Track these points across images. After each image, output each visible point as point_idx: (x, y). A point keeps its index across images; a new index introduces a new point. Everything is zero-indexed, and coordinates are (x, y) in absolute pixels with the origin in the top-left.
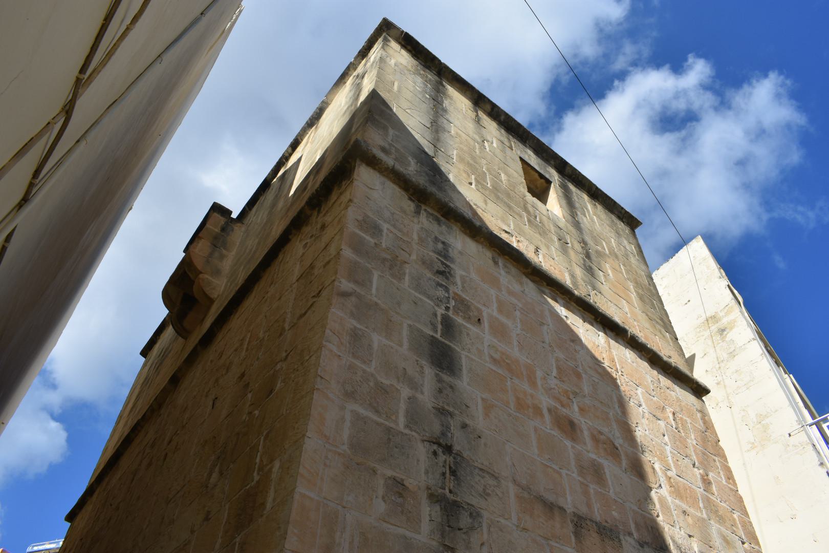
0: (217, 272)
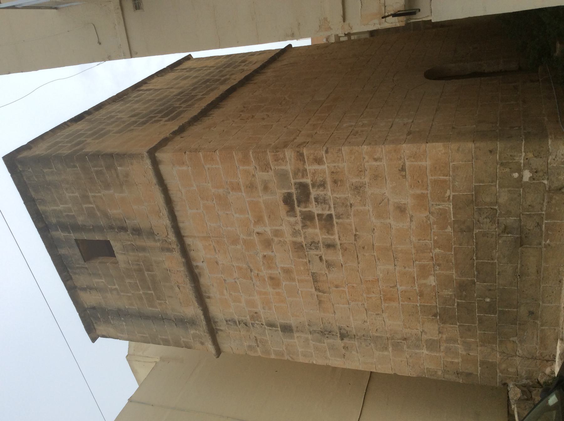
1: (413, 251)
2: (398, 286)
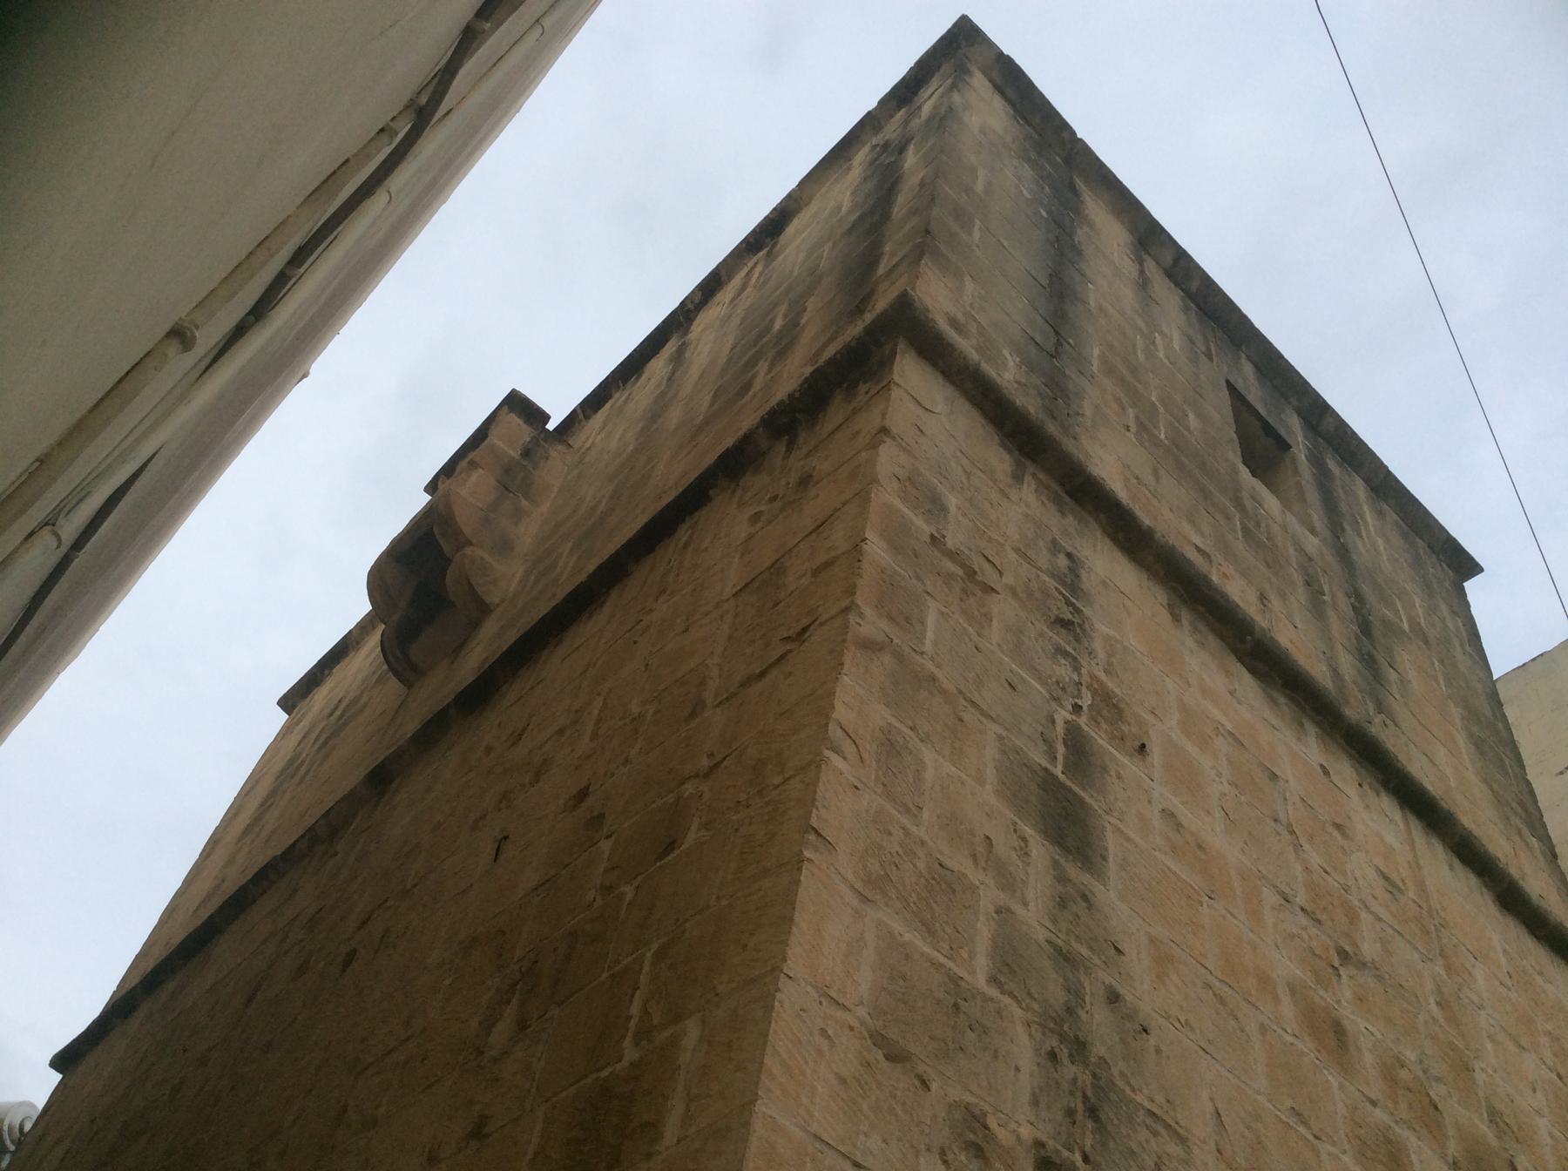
0: (504, 547)
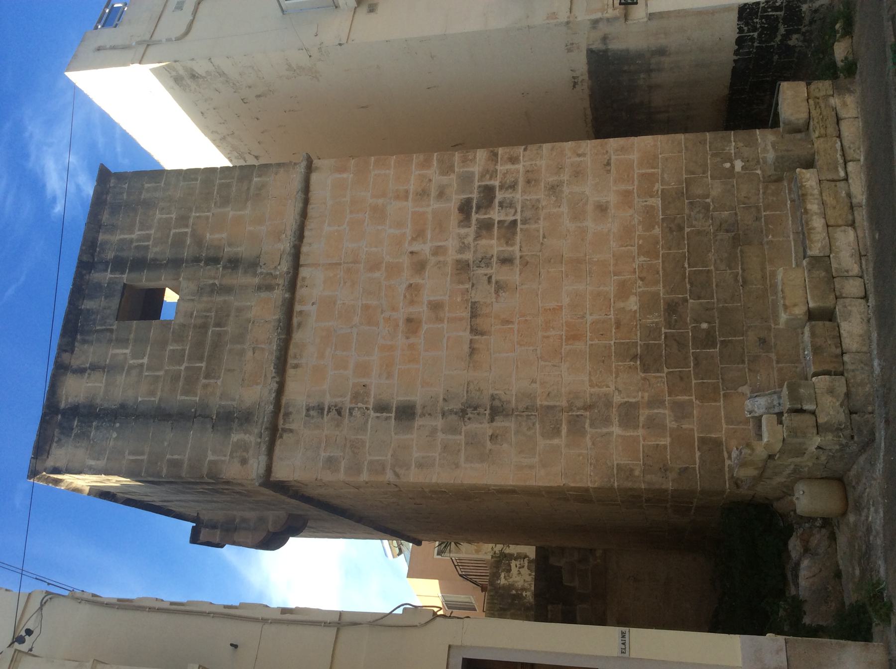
0: (262, 520)
1: (612, 262)
2: (588, 316)
